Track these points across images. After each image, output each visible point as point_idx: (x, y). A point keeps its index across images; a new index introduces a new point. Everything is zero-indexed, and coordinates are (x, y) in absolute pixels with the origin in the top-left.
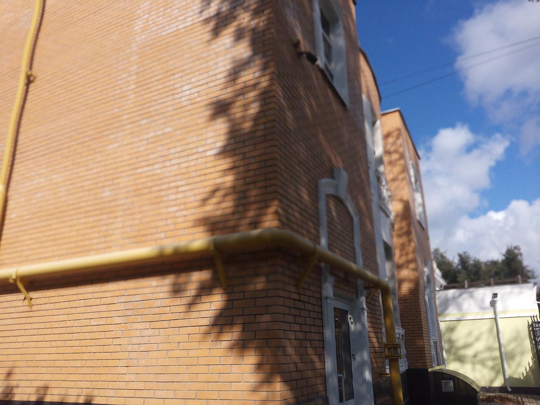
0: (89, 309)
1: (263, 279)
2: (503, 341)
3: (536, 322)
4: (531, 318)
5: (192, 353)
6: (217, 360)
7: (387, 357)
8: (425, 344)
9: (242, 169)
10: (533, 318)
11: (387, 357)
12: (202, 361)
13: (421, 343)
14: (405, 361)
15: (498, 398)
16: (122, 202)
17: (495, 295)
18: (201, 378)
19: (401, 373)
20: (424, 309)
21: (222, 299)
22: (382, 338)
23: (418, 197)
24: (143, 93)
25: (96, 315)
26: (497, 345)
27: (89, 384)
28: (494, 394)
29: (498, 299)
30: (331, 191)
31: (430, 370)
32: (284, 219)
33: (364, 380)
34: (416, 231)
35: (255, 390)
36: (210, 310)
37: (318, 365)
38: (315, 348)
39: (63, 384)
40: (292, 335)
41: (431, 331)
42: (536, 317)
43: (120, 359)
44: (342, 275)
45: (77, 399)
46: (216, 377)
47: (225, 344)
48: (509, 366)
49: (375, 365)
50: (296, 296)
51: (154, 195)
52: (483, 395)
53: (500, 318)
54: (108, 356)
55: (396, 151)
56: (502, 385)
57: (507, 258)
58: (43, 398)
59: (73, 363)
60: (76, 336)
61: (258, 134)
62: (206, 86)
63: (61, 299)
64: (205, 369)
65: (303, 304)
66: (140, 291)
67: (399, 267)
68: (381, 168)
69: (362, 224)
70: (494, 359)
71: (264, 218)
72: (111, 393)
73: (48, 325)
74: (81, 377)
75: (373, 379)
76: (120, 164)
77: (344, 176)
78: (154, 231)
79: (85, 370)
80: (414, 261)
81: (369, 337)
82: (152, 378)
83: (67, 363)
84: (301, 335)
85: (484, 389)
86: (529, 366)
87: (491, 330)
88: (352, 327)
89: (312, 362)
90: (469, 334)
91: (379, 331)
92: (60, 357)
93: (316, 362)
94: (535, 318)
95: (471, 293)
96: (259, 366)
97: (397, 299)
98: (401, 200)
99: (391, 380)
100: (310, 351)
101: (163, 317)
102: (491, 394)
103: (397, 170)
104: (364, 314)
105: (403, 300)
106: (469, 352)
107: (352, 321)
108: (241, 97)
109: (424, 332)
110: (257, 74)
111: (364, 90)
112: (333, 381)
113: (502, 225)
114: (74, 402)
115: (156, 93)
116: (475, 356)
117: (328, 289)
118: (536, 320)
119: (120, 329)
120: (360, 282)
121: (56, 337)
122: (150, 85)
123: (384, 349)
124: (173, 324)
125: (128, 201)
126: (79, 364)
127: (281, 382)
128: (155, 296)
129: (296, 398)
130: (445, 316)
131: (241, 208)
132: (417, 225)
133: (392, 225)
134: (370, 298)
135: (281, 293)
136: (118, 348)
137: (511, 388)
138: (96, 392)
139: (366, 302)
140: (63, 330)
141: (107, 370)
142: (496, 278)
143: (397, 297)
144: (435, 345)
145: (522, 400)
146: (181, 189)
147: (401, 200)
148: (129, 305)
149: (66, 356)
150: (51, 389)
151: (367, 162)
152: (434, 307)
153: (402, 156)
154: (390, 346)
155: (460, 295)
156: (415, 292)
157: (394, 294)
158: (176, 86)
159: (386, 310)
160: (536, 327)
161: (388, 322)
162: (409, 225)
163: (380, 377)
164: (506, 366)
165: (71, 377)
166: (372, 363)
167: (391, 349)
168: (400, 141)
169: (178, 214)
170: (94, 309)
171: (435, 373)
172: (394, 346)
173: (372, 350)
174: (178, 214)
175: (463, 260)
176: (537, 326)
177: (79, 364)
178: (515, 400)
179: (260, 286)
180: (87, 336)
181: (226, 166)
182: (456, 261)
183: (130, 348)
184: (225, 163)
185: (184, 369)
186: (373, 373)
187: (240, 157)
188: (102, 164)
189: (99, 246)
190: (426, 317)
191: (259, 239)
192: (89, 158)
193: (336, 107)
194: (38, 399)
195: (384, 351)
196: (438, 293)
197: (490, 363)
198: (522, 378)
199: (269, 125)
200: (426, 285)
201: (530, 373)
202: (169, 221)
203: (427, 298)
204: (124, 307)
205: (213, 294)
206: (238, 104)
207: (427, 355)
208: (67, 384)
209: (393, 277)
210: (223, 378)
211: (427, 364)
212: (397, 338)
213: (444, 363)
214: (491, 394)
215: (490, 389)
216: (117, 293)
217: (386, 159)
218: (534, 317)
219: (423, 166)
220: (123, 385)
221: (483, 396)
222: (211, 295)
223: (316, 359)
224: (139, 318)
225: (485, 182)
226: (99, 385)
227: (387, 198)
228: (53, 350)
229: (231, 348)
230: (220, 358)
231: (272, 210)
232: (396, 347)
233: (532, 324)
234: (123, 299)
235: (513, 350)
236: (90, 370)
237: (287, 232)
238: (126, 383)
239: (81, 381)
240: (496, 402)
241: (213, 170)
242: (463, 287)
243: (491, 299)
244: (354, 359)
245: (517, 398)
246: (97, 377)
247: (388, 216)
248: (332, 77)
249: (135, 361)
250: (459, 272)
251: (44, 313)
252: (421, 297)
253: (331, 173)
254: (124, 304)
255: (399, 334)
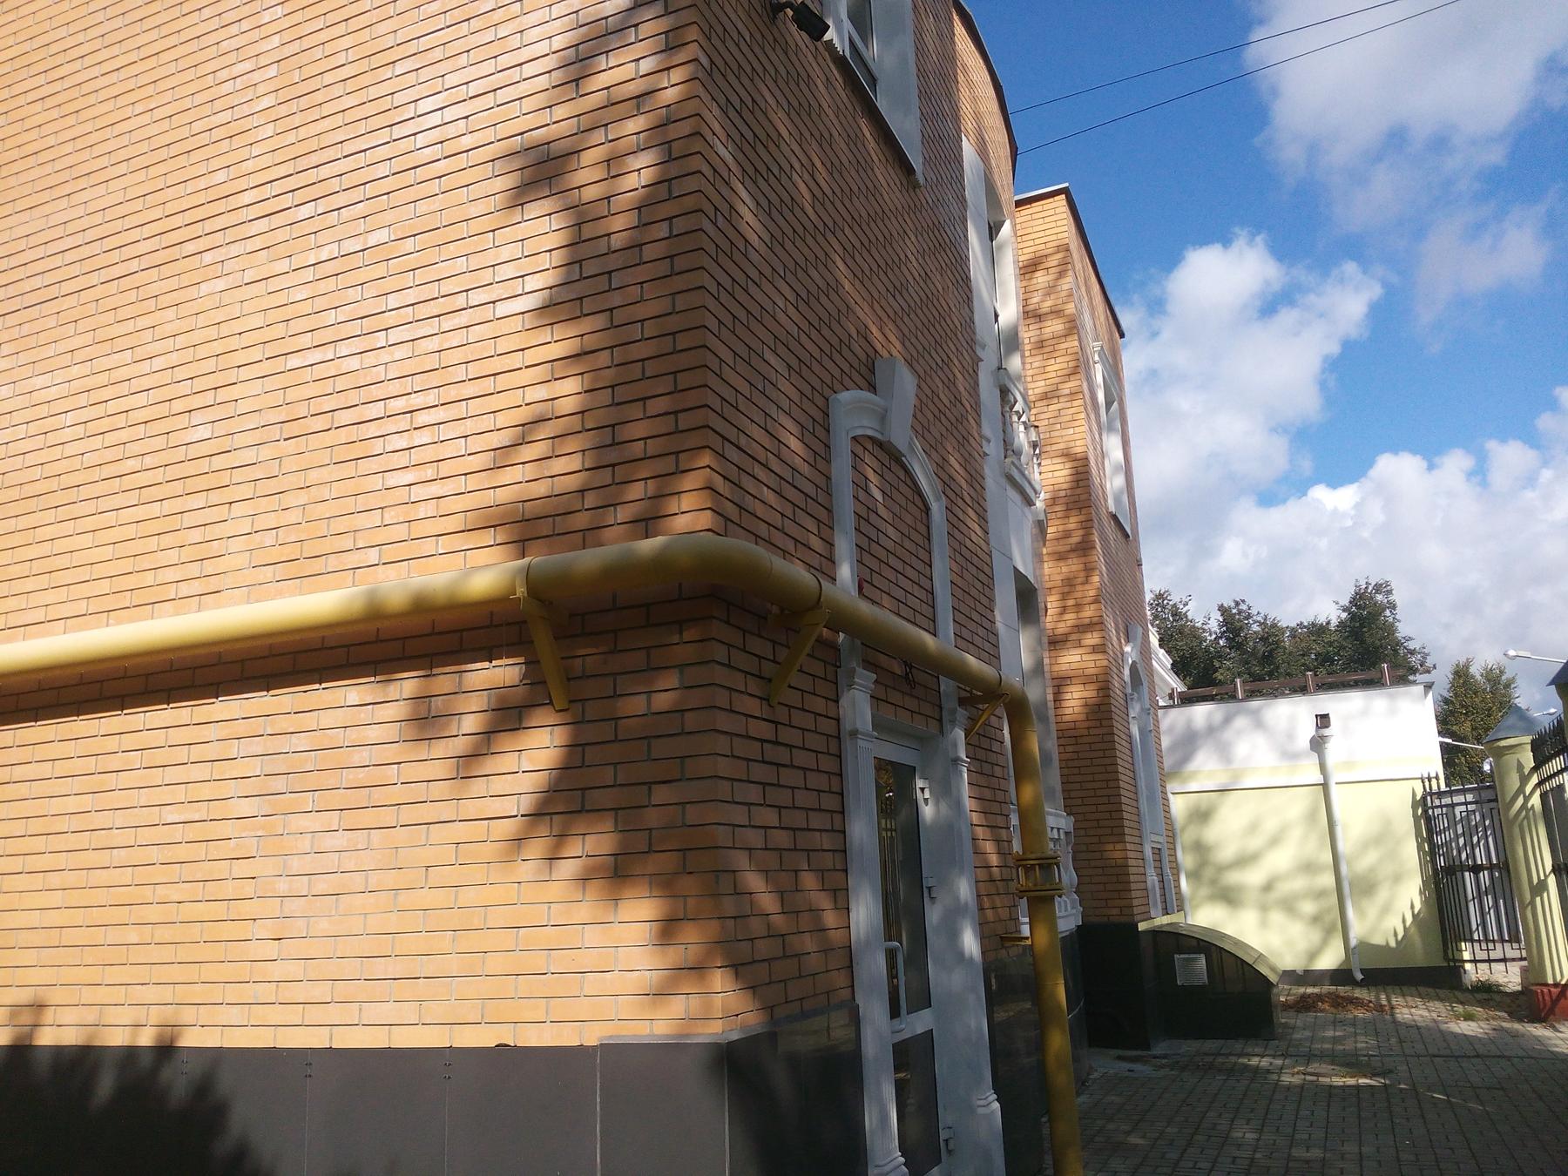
0: (157, 776)
1: (671, 680)
2: (1342, 846)
3: (1435, 794)
4: (1423, 782)
5: (469, 896)
6: (540, 914)
7: (1022, 893)
8: (1131, 854)
9: (603, 359)
10: (1427, 784)
11: (1022, 893)
12: (498, 917)
13: (1118, 855)
14: (1073, 901)
15: (1327, 999)
16: (249, 456)
17: (1323, 720)
18: (495, 964)
19: (1060, 936)
20: (1125, 757)
21: (551, 743)
22: (1010, 842)
23: (1113, 444)
24: (297, 120)
25: (180, 794)
26: (1327, 857)
27: (167, 994)
28: (1316, 990)
29: (1333, 730)
30: (867, 426)
31: (1142, 926)
32: (731, 510)
33: (960, 955)
34: (1104, 540)
35: (660, 994)
36: (517, 772)
37: (830, 919)
38: (822, 871)
39: (88, 995)
40: (755, 838)
41: (1147, 825)
42: (1437, 778)
43: (255, 920)
44: (898, 669)
45: (134, 1035)
46: (539, 961)
47: (568, 868)
48: (1361, 913)
49: (989, 913)
50: (765, 730)
51: (343, 435)
52: (1286, 993)
53: (1336, 783)
54: (219, 910)
55: (1056, 312)
56: (1341, 965)
57: (1353, 617)
58: (30, 1036)
59: (113, 935)
60: (120, 856)
61: (649, 252)
62: (489, 100)
63: (69, 748)
64: (507, 939)
65: (729, 738)
66: (309, 721)
67: (1056, 643)
68: (1015, 363)
69: (955, 524)
70: (1320, 894)
71: (672, 506)
72: (235, 1015)
73: (36, 826)
74: (142, 973)
75: (983, 953)
76: (234, 343)
77: (906, 384)
78: (346, 542)
79: (156, 954)
80: (1096, 625)
81: (973, 839)
82: (350, 968)
83: (99, 935)
84: (782, 839)
85: (1291, 976)
86: (1413, 912)
87: (1311, 817)
88: (928, 811)
89: (816, 912)
90: (1253, 828)
91: (1000, 821)
92: (78, 917)
93: (823, 910)
94: (1434, 782)
95: (1256, 713)
96: (667, 930)
97: (1054, 735)
98: (1067, 455)
99: (1033, 956)
100: (809, 880)
101: (378, 796)
102: (1310, 990)
103: (1057, 366)
104: (961, 776)
105: (1069, 736)
106: (1252, 877)
107: (927, 795)
108: (598, 136)
109: (1126, 823)
110: (646, 66)
111: (968, 124)
112: (873, 966)
113: (1349, 523)
114: (79, 1044)
115: (338, 120)
116: (1268, 887)
117: (858, 707)
118: (1435, 788)
119: (253, 834)
120: (946, 685)
121: (61, 861)
122: (319, 97)
123: (1014, 871)
124: (408, 815)
125: (266, 452)
126: (133, 936)
127: (726, 967)
128: (354, 737)
129: (769, 1009)
130: (1184, 781)
131: (605, 476)
132: (1106, 521)
133: (1041, 527)
134: (979, 734)
135: (724, 722)
136: (248, 889)
137: (1362, 971)
138: (188, 1015)
139: (967, 744)
140: (83, 840)
141: (218, 951)
142: (1322, 671)
143: (1053, 727)
144: (1157, 857)
145: (1389, 1000)
146: (423, 418)
147: (1067, 455)
148: (279, 765)
149: (97, 915)
150: (55, 1010)
151: (972, 342)
152: (1156, 759)
153: (1073, 327)
154: (1032, 862)
155: (1227, 720)
156: (1102, 712)
157: (1044, 719)
158: (400, 99)
159: (1023, 768)
160: (1433, 808)
161: (1028, 792)
162: (1087, 526)
163: (1003, 947)
164: (1351, 913)
165: (115, 975)
166: (981, 909)
167: (1035, 870)
168: (1067, 283)
169: (419, 492)
170: (173, 774)
171: (1156, 933)
172: (1025, 863)
173: (982, 874)
174: (419, 492)
175: (1233, 622)
176: (1437, 802)
177: (133, 936)
178: (1370, 1002)
179: (663, 701)
180: (154, 854)
181: (557, 350)
182: (1214, 624)
183: (283, 886)
184: (558, 342)
185: (445, 942)
186: (983, 938)
187: (599, 321)
188: (181, 341)
189: (185, 589)
190: (1132, 782)
191: (660, 565)
192: (142, 322)
193: (884, 175)
194: (18, 1038)
195: (1014, 876)
196: (1165, 714)
197: (1308, 907)
198: (1393, 944)
199: (680, 225)
200: (1129, 690)
201: (1413, 930)
202: (389, 516)
203: (1135, 730)
204: (262, 766)
205: (524, 726)
206: (588, 157)
207: (1133, 886)
208: (102, 994)
209: (1038, 669)
210: (560, 961)
211: (1136, 911)
212: (1052, 839)
213: (1181, 908)
214: (1310, 990)
215: (1308, 977)
216: (241, 728)
217: (1027, 335)
218: (1430, 779)
219: (1133, 361)
220: (265, 992)
221: (1288, 995)
222: (518, 729)
223: (823, 901)
224: (308, 801)
225: (1306, 402)
226: (198, 993)
227: (1026, 448)
228: (57, 899)
229: (584, 879)
230: (550, 907)
231: (690, 481)
232: (1048, 865)
233: (1424, 798)
234: (257, 746)
235: (1372, 870)
236: (166, 953)
237: (739, 545)
238: (277, 986)
239: (142, 984)
240: (1321, 1011)
241: (516, 360)
242: (1232, 697)
243: (1313, 733)
244: (932, 899)
245: (1378, 998)
246: (192, 973)
247: (1030, 503)
248: (873, 81)
249: (301, 923)
250: (1220, 656)
251: (23, 790)
252: (1120, 727)
253: (868, 376)
254: (262, 760)
255: (1058, 829)
